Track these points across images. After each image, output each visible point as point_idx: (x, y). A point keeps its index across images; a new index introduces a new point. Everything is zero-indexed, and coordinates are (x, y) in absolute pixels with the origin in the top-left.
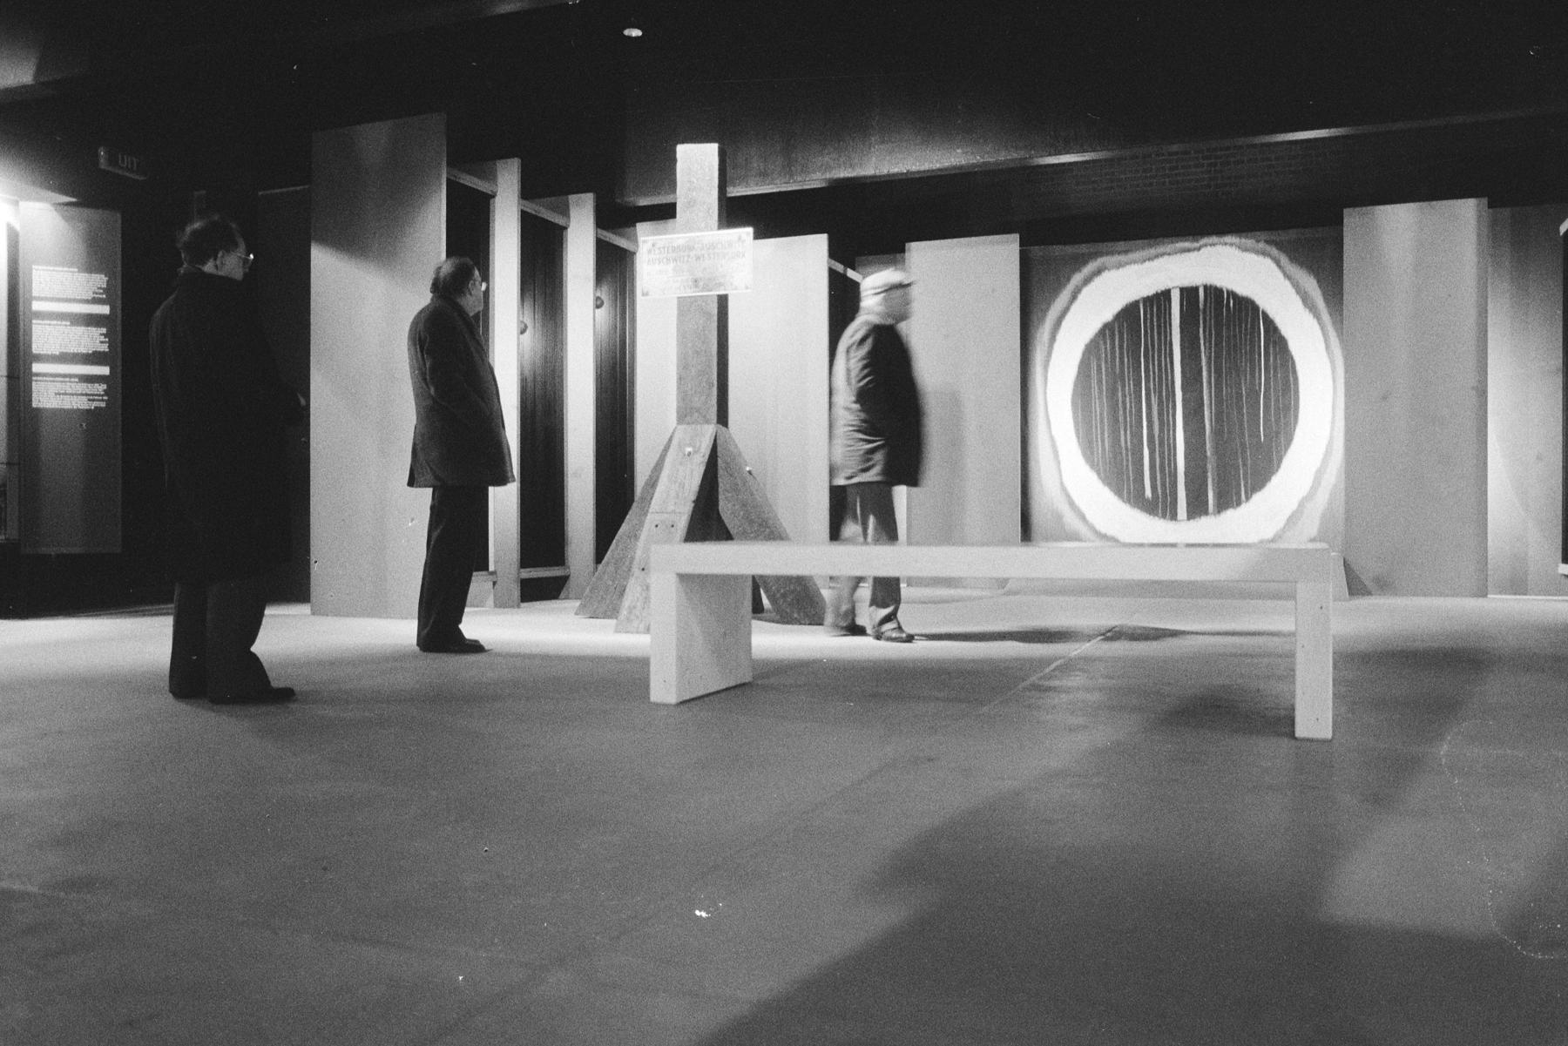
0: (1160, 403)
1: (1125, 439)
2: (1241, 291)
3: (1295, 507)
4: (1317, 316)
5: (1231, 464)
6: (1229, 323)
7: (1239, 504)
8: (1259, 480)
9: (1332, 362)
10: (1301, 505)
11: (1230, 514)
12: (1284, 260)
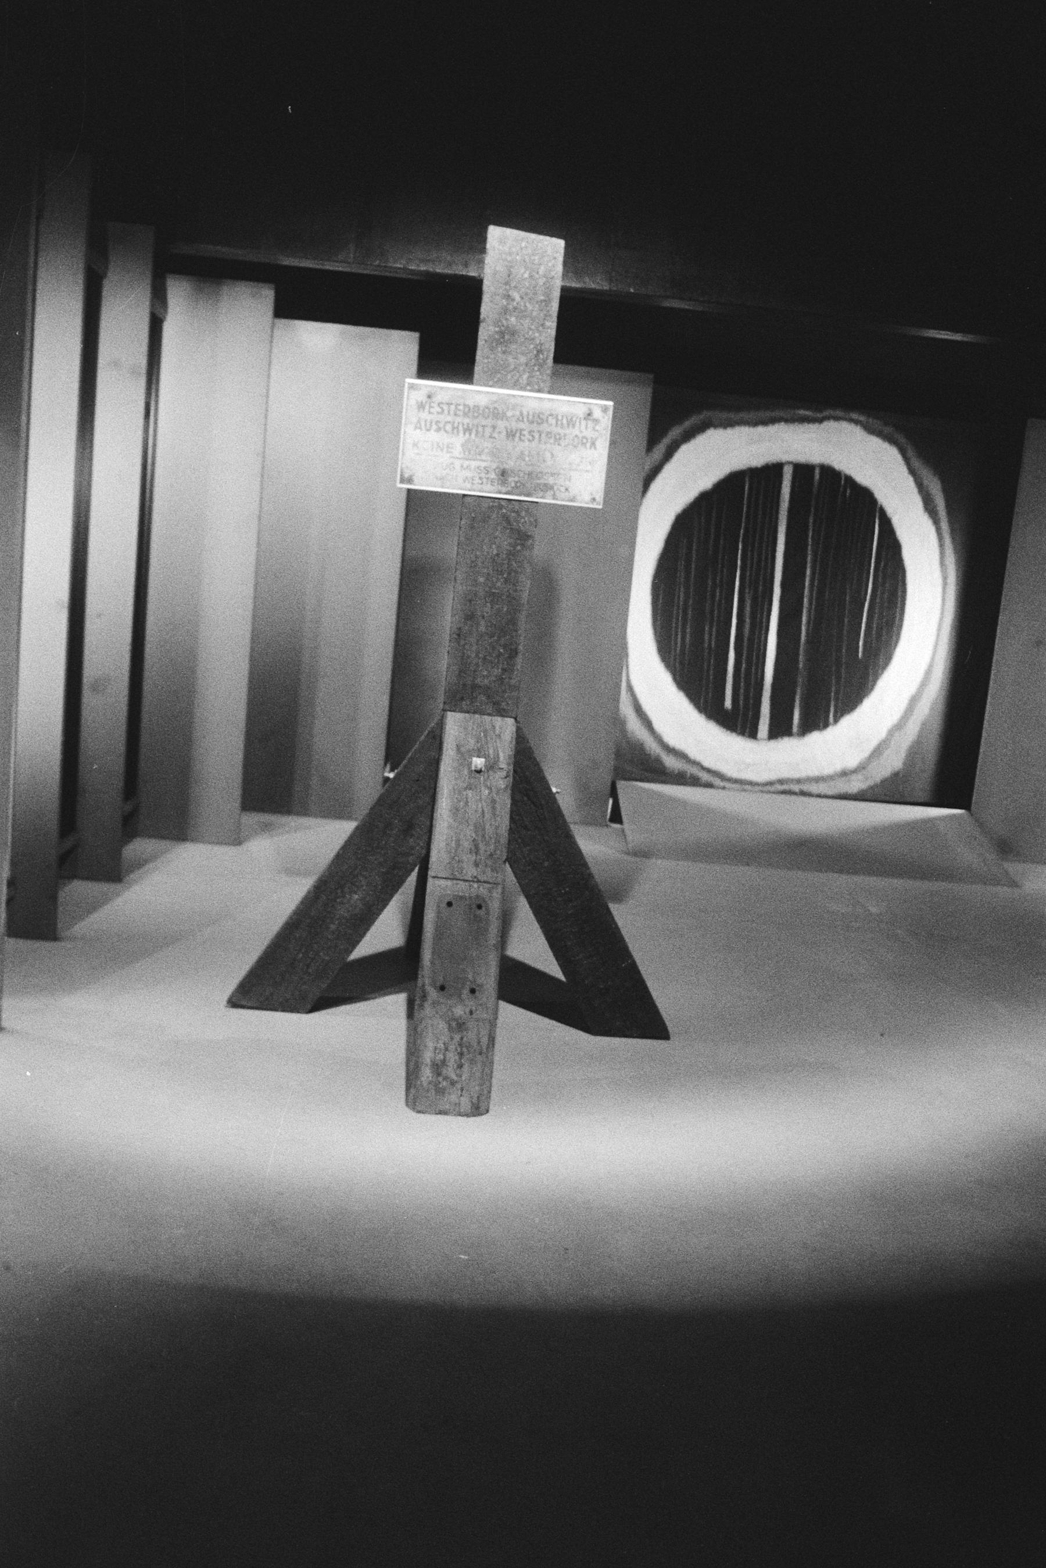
0: (754, 599)
1: (709, 639)
2: (848, 472)
3: (883, 734)
4: (936, 522)
5: (825, 682)
6: (841, 513)
7: (826, 725)
8: (850, 701)
9: (945, 578)
10: (891, 733)
11: (815, 737)
12: (910, 453)
